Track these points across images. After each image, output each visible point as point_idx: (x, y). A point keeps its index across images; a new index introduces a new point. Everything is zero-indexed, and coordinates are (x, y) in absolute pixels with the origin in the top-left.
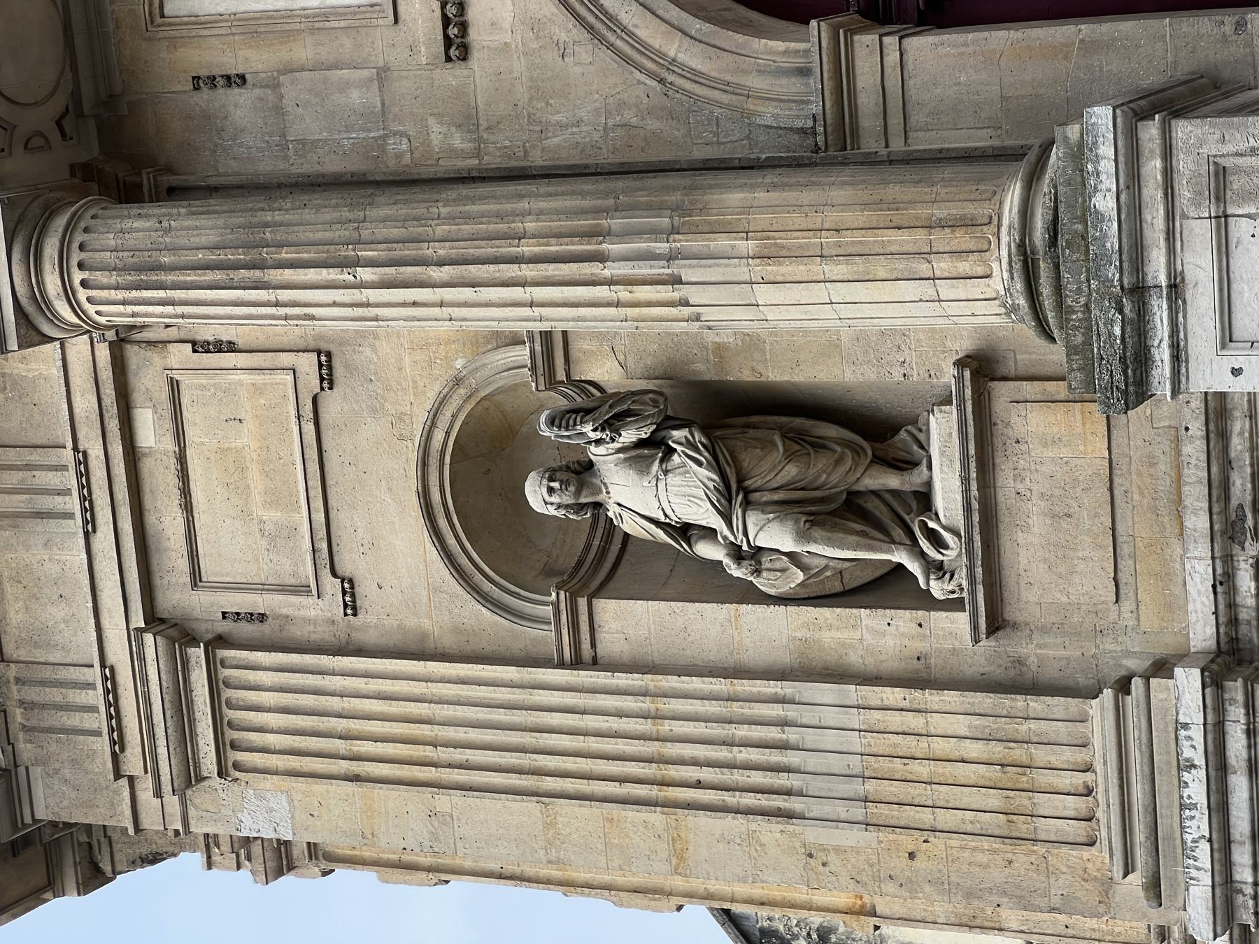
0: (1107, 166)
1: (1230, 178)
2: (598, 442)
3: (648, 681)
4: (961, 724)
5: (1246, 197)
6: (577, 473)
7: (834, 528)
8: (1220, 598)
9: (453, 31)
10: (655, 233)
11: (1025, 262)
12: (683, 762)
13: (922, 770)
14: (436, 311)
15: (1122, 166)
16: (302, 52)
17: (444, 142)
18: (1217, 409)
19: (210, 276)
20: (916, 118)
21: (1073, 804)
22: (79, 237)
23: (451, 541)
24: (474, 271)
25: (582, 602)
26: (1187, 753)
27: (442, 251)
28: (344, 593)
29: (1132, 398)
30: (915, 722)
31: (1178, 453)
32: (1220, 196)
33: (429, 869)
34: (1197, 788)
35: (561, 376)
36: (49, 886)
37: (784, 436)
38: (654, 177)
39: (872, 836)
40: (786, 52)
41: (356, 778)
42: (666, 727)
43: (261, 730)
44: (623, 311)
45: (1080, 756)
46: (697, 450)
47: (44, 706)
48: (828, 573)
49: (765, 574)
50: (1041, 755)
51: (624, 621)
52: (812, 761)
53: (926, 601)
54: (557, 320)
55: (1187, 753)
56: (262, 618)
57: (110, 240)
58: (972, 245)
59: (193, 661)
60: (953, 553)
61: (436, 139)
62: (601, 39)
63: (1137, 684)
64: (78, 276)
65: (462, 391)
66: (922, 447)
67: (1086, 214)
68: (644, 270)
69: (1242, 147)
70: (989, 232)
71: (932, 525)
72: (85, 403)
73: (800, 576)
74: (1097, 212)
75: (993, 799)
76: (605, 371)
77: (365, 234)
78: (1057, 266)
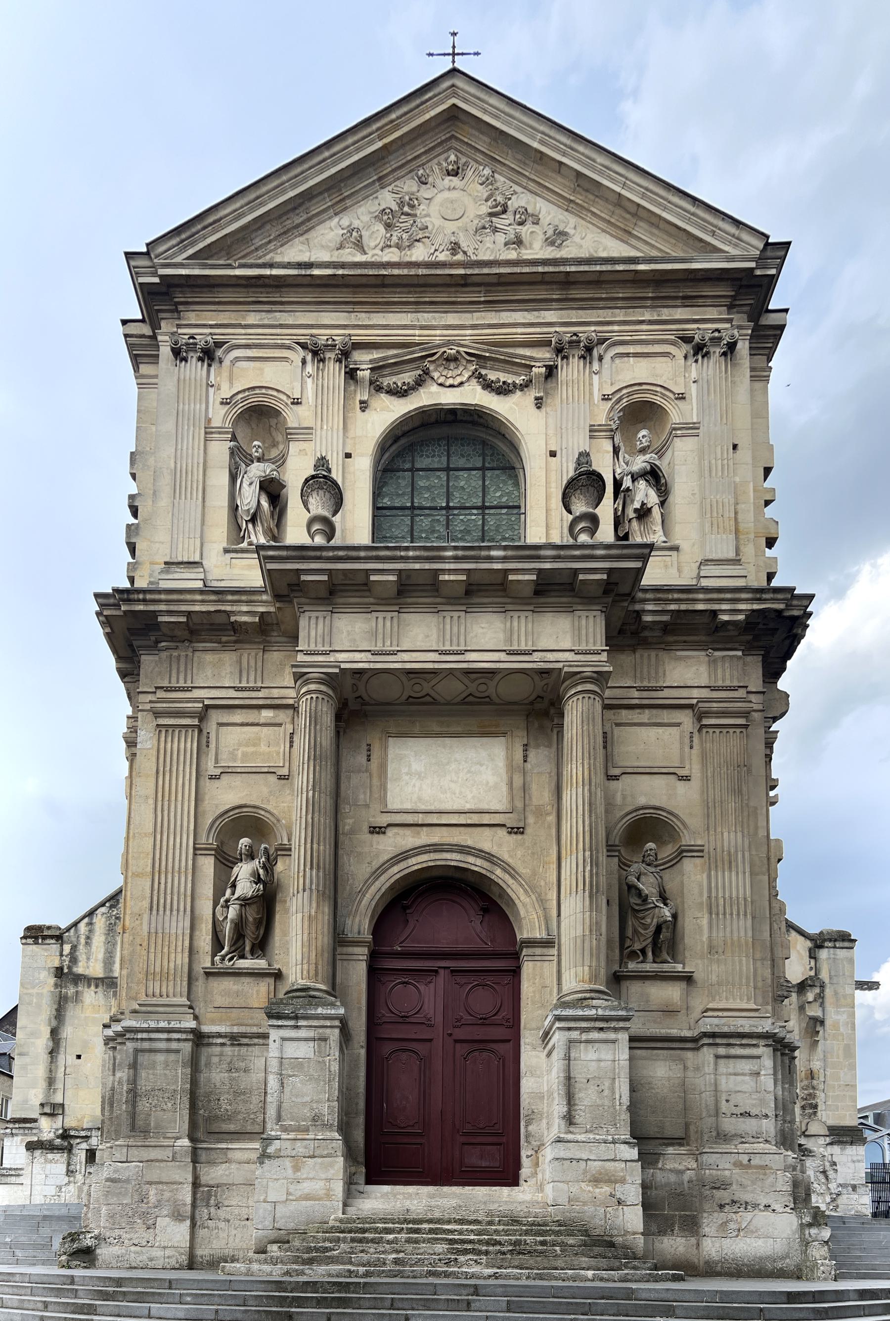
0: (329, 1012)
4: (179, 962)
5: (319, 1046)
7: (234, 930)
10: (318, 885)
13: (166, 950)
16: (375, 781)
17: (347, 823)
18: (265, 1036)
20: (345, 963)
21: (157, 992)
23: (231, 813)
24: (310, 829)
27: (316, 819)
30: (179, 949)
32: (319, 1039)
34: (163, 1024)
35: (279, 853)
36: (119, 658)
38: (334, 888)
39: (146, 934)
41: (157, 772)
42: (176, 875)
45: (171, 994)
47: (178, 664)
50: (171, 983)
51: (208, 865)
53: (214, 955)
54: (295, 854)
56: (208, 746)
57: (325, 709)
62: (372, 875)
63: (192, 1011)
67: (317, 1005)
72: (275, 693)
73: (221, 919)
75: (158, 970)
76: (280, 867)
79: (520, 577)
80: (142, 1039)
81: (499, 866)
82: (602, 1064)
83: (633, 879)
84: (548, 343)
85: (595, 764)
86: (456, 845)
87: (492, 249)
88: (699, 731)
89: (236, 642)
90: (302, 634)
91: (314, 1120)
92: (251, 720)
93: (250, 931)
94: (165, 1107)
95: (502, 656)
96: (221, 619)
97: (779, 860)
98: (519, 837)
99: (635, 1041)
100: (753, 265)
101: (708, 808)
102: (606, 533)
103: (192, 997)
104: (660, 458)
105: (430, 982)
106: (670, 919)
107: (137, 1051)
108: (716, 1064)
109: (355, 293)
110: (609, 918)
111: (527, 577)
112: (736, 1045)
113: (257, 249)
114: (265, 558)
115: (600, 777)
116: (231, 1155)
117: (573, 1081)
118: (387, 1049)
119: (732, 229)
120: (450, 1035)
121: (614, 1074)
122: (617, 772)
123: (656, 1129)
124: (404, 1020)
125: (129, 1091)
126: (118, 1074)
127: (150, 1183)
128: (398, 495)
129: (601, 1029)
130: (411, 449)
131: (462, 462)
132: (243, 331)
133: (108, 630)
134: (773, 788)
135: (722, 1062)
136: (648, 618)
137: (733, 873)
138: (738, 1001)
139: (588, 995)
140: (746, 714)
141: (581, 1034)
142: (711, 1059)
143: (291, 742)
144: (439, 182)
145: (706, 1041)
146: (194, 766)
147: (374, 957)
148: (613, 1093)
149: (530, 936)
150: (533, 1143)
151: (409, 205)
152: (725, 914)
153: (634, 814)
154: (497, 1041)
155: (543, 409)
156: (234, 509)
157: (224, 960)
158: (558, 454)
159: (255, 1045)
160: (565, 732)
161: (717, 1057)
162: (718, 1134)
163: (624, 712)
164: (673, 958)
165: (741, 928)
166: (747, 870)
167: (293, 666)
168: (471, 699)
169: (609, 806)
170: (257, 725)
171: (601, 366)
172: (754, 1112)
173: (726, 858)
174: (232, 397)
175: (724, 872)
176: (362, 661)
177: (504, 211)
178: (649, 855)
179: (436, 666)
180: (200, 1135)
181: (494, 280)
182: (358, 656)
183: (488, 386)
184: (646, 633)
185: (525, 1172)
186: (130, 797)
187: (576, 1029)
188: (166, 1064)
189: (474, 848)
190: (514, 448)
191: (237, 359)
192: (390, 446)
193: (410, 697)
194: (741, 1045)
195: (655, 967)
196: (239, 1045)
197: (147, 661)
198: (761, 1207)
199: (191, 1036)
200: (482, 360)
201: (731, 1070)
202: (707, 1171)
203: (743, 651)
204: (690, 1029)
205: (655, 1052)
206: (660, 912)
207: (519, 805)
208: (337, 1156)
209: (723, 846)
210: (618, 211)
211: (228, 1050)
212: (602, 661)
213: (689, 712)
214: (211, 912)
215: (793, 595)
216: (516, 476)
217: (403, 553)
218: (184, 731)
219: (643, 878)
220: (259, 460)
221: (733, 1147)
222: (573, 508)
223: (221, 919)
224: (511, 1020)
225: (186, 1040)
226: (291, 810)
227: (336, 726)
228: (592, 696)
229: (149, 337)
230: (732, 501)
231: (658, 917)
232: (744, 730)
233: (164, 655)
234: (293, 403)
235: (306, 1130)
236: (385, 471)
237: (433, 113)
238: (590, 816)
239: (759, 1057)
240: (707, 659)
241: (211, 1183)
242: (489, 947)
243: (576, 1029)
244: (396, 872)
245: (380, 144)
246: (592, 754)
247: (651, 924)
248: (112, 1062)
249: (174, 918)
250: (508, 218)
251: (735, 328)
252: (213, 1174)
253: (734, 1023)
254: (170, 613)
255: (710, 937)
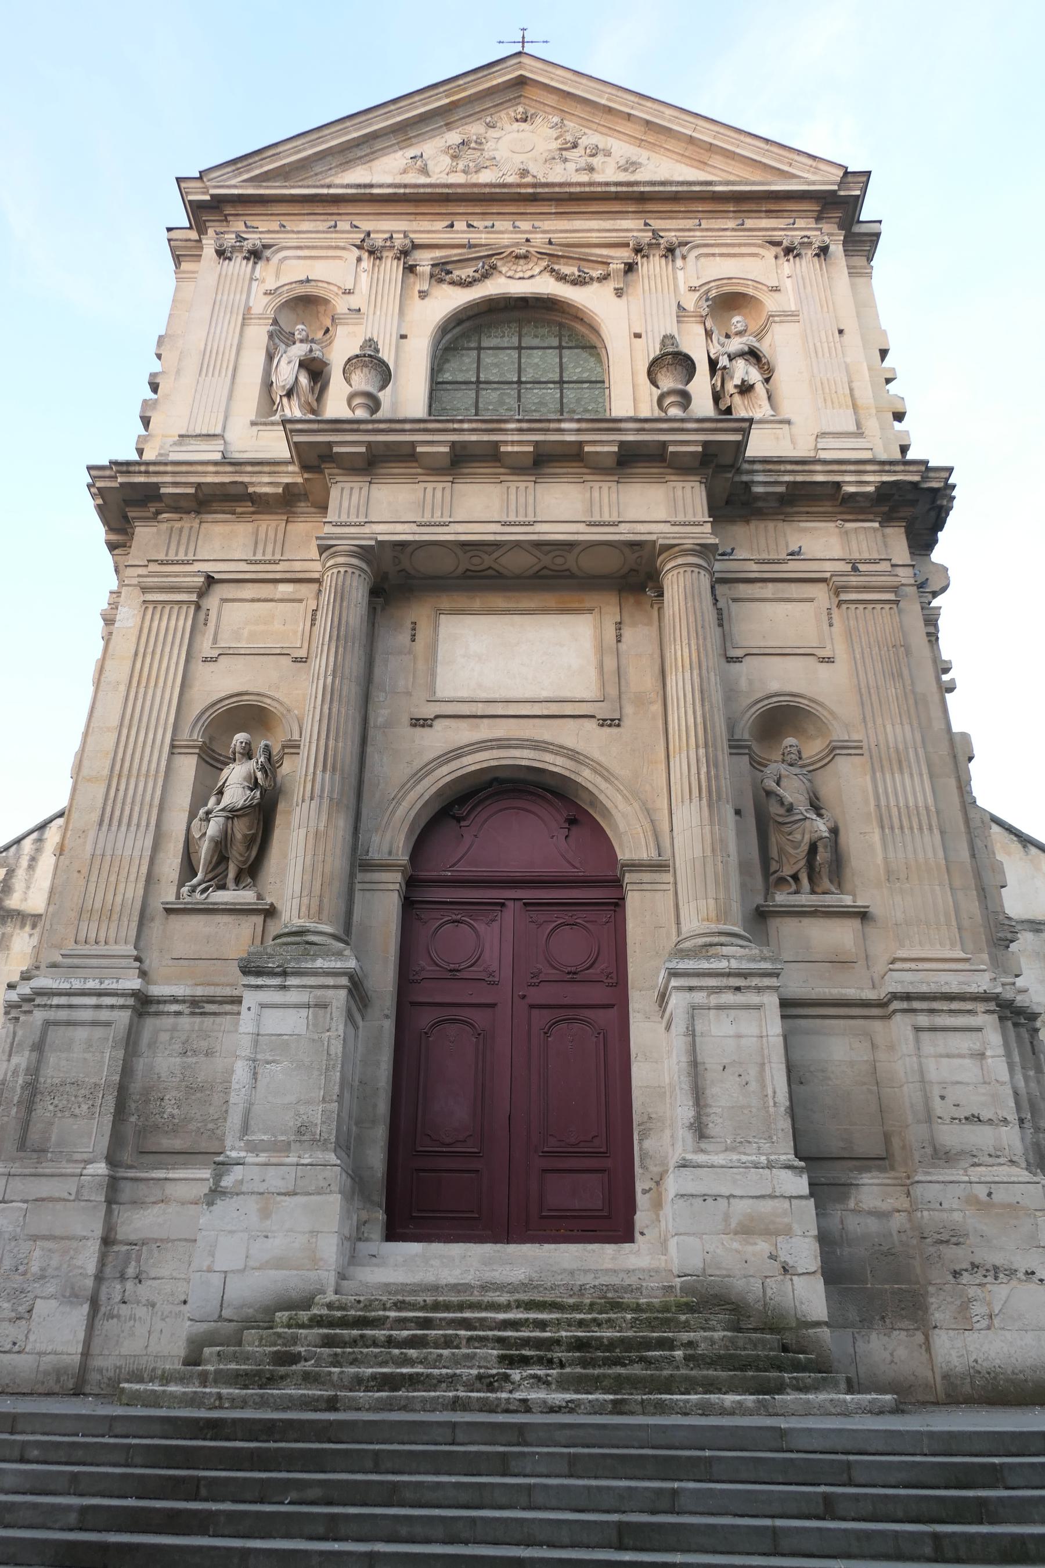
0: (333, 965)
3: (162, 774)
4: (130, 894)
5: (315, 1016)
7: (214, 851)
9: (609, 722)
10: (332, 791)
12: (127, 784)
13: (113, 878)
14: (312, 705)
16: (421, 665)
17: (380, 715)
18: (238, 1001)
19: (336, 620)
21: (92, 936)
22: (357, 572)
23: (227, 702)
25: (197, 751)
26: (107, 982)
27: (335, 710)
30: (132, 877)
31: (227, 985)
32: (316, 1006)
33: (99, 679)
34: (91, 984)
35: (286, 751)
36: (111, 528)
38: (357, 794)
39: (88, 856)
41: (136, 654)
42: (142, 779)
43: (160, 619)
45: (111, 940)
47: (180, 536)
50: (114, 925)
51: (188, 766)
52: (121, 835)
53: (181, 884)
54: (304, 751)
55: (107, 982)
56: (206, 624)
57: (355, 584)
60: (198, 896)
63: (137, 964)
64: (342, 570)
68: (318, 786)
72: (298, 566)
75: (98, 905)
76: (285, 768)
77: (346, 681)
79: (599, 449)
80: (58, 1006)
81: (587, 766)
82: (743, 1041)
83: (771, 784)
84: (627, 245)
85: (705, 646)
86: (528, 740)
87: (559, 174)
88: (839, 606)
89: (253, 513)
90: (333, 504)
91: (299, 1132)
94: (77, 1111)
95: (582, 527)
96: (240, 490)
97: (970, 759)
99: (791, 1007)
100: (835, 188)
102: (703, 405)
103: (142, 944)
104: (759, 341)
106: (826, 834)
108: (917, 1041)
109: (416, 206)
111: (606, 449)
112: (942, 1011)
113: (316, 174)
114: (291, 431)
115: (713, 659)
116: (171, 1189)
117: (700, 1068)
118: (425, 1019)
119: (810, 162)
120: (524, 997)
121: (763, 1056)
122: (739, 653)
123: (842, 1144)
124: (453, 974)
125: (27, 1085)
126: (15, 1060)
127: (35, 1238)
128: (461, 371)
129: (738, 989)
130: (478, 330)
131: (536, 342)
132: (295, 236)
133: (100, 501)
134: (946, 671)
135: (925, 1036)
136: (759, 489)
137: (906, 776)
138: (938, 946)
139: (716, 940)
140: (895, 589)
141: (709, 996)
142: (910, 1034)
143: (313, 620)
144: (507, 127)
145: (896, 1005)
147: (412, 883)
148: (763, 1086)
150: (652, 1168)
151: (476, 142)
152: (902, 828)
153: (766, 702)
154: (594, 1004)
155: (624, 298)
156: (268, 385)
157: (194, 891)
158: (643, 335)
159: (226, 1014)
161: (918, 1029)
162: (935, 1149)
163: (742, 587)
164: (840, 886)
165: (928, 847)
166: (925, 771)
167: (317, 538)
168: (469, 573)
169: (730, 693)
170: (271, 600)
171: (685, 264)
172: (985, 1115)
173: (893, 756)
174: (277, 289)
175: (893, 774)
176: (404, 533)
177: (575, 146)
178: (790, 753)
179: (499, 538)
180: (127, 1156)
181: (566, 196)
182: (399, 528)
183: (562, 278)
184: (760, 504)
185: (641, 1218)
186: (98, 684)
187: (701, 988)
188: (89, 1044)
189: (552, 744)
190: (595, 330)
191: (286, 258)
192: (454, 327)
193: (468, 570)
194: (951, 1011)
197: (143, 533)
198: (1021, 1275)
199: (131, 1001)
200: (552, 258)
201: (941, 1050)
202: (926, 1213)
203: (880, 522)
204: (874, 987)
205: (828, 1021)
206: (812, 826)
207: (613, 691)
208: (331, 1192)
209: (887, 741)
210: (690, 147)
211: (185, 1022)
212: (705, 533)
213: (822, 586)
215: (927, 467)
216: (598, 354)
217: (456, 426)
218: (176, 607)
219: (784, 782)
220: (302, 341)
221: (961, 1172)
222: (660, 384)
224: (614, 975)
225: (122, 1007)
226: (303, 698)
227: (370, 603)
228: (696, 570)
229: (196, 241)
230: (845, 379)
231: (811, 832)
232: (894, 606)
233: (164, 526)
234: (344, 293)
235: (286, 1148)
236: (447, 349)
237: (500, 80)
238: (703, 705)
239: (979, 1029)
240: (837, 530)
241: (133, 1237)
242: (563, 869)
243: (701, 988)
244: (446, 774)
245: (447, 101)
246: (700, 633)
248: (9, 1041)
249: (131, 835)
250: (579, 151)
251: (831, 235)
252: (137, 1223)
253: (935, 979)
254: (176, 484)
255: (885, 858)
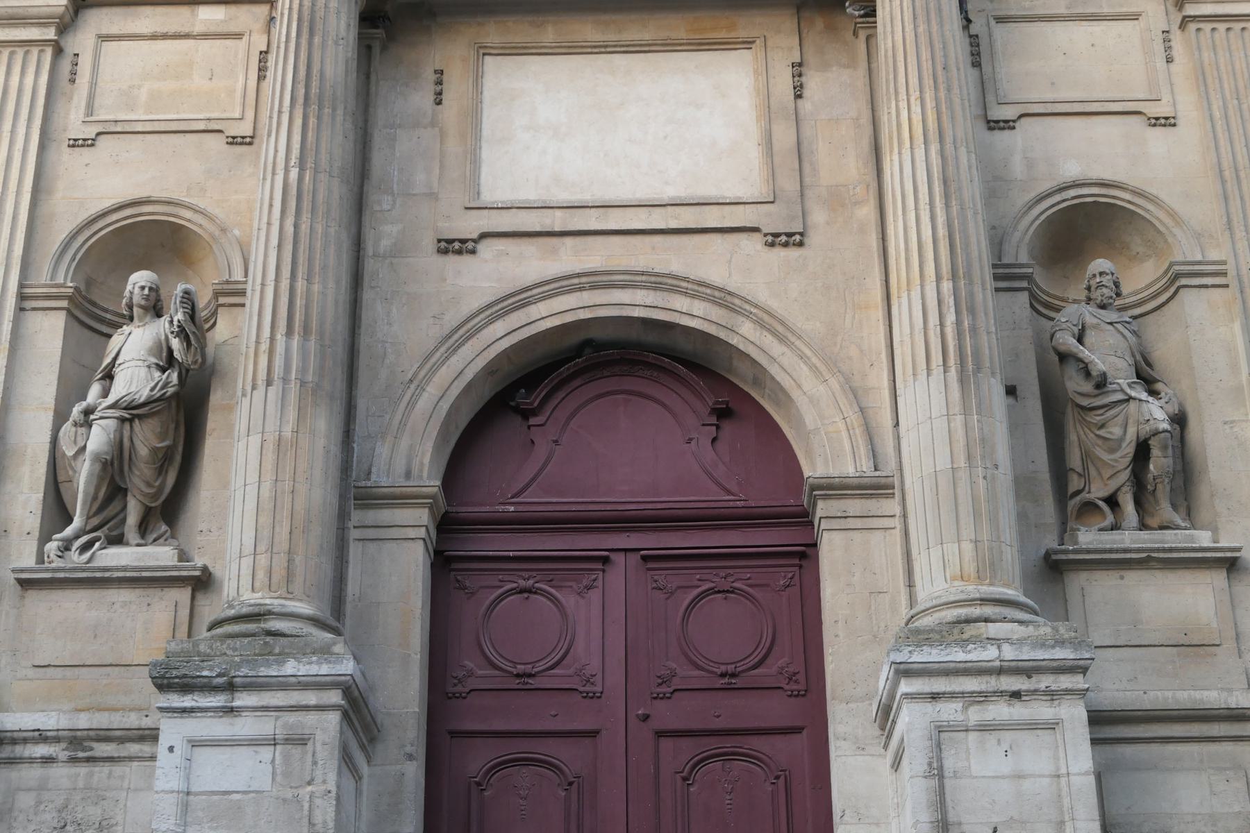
0: (314, 669)
1: (299, 748)
2: (171, 322)
5: (287, 758)
6: (154, 307)
7: (101, 479)
8: (31, 734)
10: (303, 370)
11: (259, 615)
14: (265, 220)
15: (313, 679)
16: (453, 146)
17: (384, 233)
18: (152, 736)
20: (372, 547)
23: (115, 217)
24: (289, 248)
25: (65, 304)
27: (304, 227)
28: (84, 140)
29: (159, 681)
32: (288, 741)
37: (168, 447)
38: (347, 373)
40: (422, 464)
44: (252, 345)
46: (162, 388)
48: (71, 473)
49: (74, 429)
51: (49, 331)
53: (45, 538)
54: (252, 301)
56: (73, 81)
58: (274, 580)
59: (45, 30)
60: (76, 558)
61: (388, 228)
62: (442, 343)
65: (217, 233)
66: (155, 540)
67: (282, 657)
69: (319, 756)
70: (282, 592)
71: (97, 545)
73: (70, 453)
74: (285, 662)
76: (222, 331)
78: (253, 635)
82: (1027, 784)
83: (1067, 341)
85: (950, 101)
88: (1183, 26)
92: (172, 28)
93: (140, 481)
98: (793, 253)
99: (1102, 721)
101: (1223, 182)
105: (589, 588)
107: (941, 729)
110: (1015, 427)
115: (964, 124)
120: (646, 718)
121: (1062, 812)
122: (1008, 113)
124: (523, 682)
129: (1016, 695)
139: (976, 611)
141: (965, 708)
143: (262, 70)
146: (37, 122)
149: (833, 472)
153: (1057, 198)
157: (67, 549)
159: (131, 759)
160: (880, 37)
164: (1189, 514)
169: (995, 184)
170: (187, 36)
187: (953, 696)
189: (685, 279)
195: (1147, 539)
196: (89, 760)
205: (1171, 748)
207: (789, 185)
211: (61, 774)
214: (46, 438)
218: (20, 52)
219: (1090, 338)
223: (70, 453)
224: (801, 677)
226: (249, 206)
227: (361, 37)
238: (947, 206)
243: (953, 696)
244: (501, 335)
246: (941, 79)
247: (1122, 439)
